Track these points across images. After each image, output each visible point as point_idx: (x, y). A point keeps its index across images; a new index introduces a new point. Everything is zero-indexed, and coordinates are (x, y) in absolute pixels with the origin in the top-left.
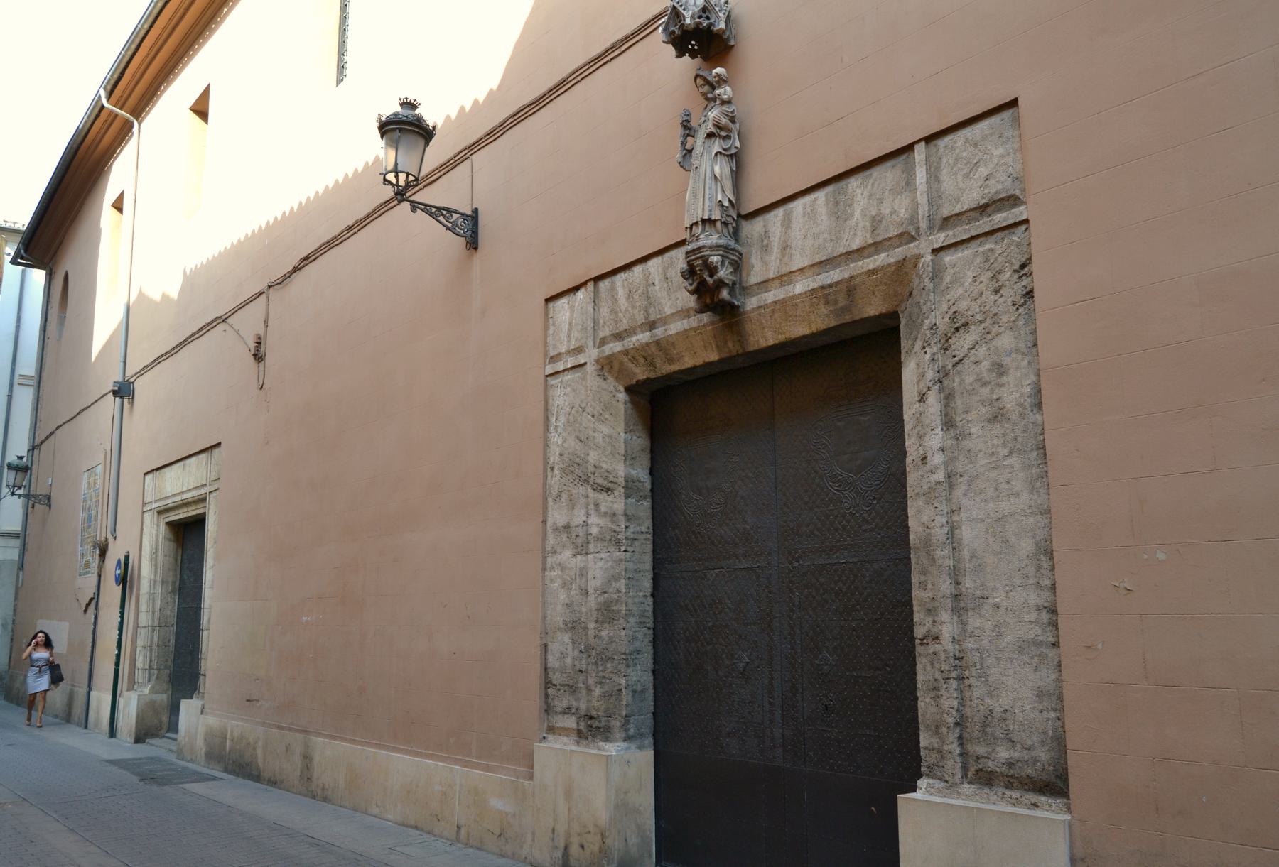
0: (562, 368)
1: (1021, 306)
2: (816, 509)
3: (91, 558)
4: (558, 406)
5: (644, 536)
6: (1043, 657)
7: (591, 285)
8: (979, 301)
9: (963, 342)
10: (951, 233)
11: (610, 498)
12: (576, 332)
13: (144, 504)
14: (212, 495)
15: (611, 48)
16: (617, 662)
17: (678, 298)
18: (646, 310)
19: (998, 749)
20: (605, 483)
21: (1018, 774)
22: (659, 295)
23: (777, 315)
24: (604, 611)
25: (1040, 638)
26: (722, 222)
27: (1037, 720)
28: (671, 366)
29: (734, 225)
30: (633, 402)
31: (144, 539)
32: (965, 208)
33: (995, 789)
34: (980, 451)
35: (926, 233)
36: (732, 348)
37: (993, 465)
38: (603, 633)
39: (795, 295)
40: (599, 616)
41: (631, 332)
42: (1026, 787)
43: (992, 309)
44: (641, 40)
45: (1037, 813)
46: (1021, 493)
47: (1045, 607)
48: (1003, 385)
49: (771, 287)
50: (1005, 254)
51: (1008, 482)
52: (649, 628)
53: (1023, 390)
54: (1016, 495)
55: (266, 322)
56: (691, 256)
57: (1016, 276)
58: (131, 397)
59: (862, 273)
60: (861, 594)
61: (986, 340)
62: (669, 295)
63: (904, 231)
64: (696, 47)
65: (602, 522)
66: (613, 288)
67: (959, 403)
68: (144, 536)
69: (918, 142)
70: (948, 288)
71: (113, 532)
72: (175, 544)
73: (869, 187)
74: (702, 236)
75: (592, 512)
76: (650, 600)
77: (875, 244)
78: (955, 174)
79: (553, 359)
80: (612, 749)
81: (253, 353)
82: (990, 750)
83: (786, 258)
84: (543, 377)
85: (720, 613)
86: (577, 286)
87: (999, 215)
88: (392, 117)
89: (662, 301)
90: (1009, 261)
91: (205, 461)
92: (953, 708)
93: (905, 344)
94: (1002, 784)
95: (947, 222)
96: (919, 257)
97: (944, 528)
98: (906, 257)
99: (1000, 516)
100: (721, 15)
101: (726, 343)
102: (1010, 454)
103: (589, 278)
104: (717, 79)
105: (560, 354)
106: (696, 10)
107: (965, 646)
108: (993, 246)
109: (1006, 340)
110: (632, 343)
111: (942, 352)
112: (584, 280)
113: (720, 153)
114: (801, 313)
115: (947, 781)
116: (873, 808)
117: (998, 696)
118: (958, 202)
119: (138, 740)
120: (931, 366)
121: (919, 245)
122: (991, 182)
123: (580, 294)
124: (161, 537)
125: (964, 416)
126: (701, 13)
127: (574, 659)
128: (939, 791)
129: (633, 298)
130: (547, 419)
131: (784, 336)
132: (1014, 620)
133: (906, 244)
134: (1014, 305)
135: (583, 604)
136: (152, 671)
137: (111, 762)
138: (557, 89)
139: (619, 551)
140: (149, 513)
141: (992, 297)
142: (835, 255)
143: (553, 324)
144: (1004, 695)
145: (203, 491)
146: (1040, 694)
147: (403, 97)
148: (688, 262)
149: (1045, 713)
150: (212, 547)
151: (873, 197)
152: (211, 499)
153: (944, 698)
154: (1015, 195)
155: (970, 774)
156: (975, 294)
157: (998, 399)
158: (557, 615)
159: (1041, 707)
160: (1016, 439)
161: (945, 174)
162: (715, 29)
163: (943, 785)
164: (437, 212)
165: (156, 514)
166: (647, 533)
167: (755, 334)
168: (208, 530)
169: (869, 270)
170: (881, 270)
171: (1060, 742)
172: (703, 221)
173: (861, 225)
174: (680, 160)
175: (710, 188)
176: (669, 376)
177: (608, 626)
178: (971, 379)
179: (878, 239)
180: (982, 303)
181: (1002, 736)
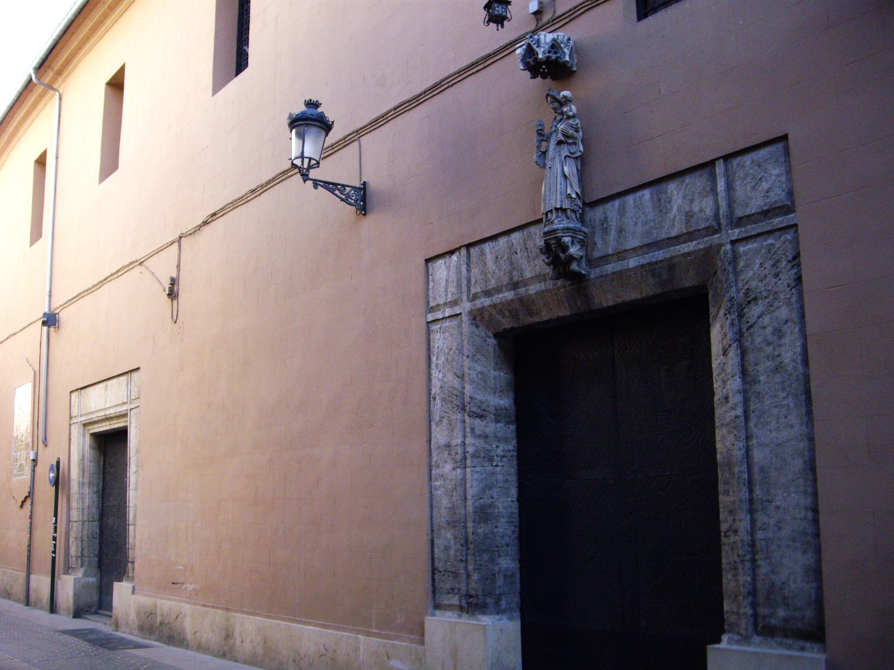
0: (441, 317)
1: (794, 287)
3: (24, 463)
5: (511, 453)
7: (464, 251)
9: (754, 311)
10: (743, 229)
12: (452, 288)
13: (71, 418)
14: (133, 412)
17: (536, 265)
18: (510, 272)
20: (479, 411)
26: (571, 210)
28: (532, 319)
29: (581, 211)
30: (499, 344)
31: (72, 448)
32: (753, 211)
34: (766, 394)
35: (725, 228)
37: (775, 405)
39: (629, 269)
41: (498, 290)
49: (610, 261)
50: (782, 248)
52: (516, 527)
53: (795, 350)
54: (792, 426)
55: (178, 267)
58: (57, 326)
61: (769, 311)
62: (528, 262)
64: (546, 70)
66: (482, 253)
67: (751, 357)
68: (72, 445)
71: (45, 442)
72: (98, 452)
74: (556, 221)
75: (468, 434)
76: (516, 504)
79: (432, 310)
80: (486, 620)
81: (167, 293)
83: (622, 239)
84: (424, 325)
87: (777, 219)
88: (299, 115)
90: (784, 254)
91: (125, 383)
92: (747, 582)
93: (712, 311)
95: (739, 222)
96: (720, 245)
100: (566, 50)
103: (462, 245)
104: (564, 99)
105: (439, 305)
106: (547, 47)
108: (773, 242)
110: (499, 299)
112: (458, 246)
113: (569, 156)
118: (747, 207)
119: (78, 613)
122: (771, 194)
123: (454, 257)
124: (86, 446)
125: (755, 367)
126: (551, 49)
127: (457, 551)
128: (737, 642)
129: (499, 263)
130: (429, 359)
131: (621, 299)
134: (789, 286)
136: (84, 558)
137: (65, 632)
139: (492, 466)
140: (77, 425)
141: (773, 279)
142: (658, 240)
143: (433, 281)
145: (124, 408)
147: (307, 99)
148: (545, 241)
150: (135, 456)
151: (686, 197)
152: (132, 415)
153: (741, 574)
154: (787, 205)
155: (759, 629)
158: (442, 515)
160: (791, 386)
161: (738, 185)
162: (561, 61)
164: (331, 186)
165: (82, 426)
166: (513, 450)
168: (130, 442)
169: (684, 253)
171: (819, 602)
172: (557, 209)
173: (677, 218)
174: (536, 160)
175: (561, 184)
176: (530, 326)
177: (483, 525)
179: (691, 230)
180: (766, 284)
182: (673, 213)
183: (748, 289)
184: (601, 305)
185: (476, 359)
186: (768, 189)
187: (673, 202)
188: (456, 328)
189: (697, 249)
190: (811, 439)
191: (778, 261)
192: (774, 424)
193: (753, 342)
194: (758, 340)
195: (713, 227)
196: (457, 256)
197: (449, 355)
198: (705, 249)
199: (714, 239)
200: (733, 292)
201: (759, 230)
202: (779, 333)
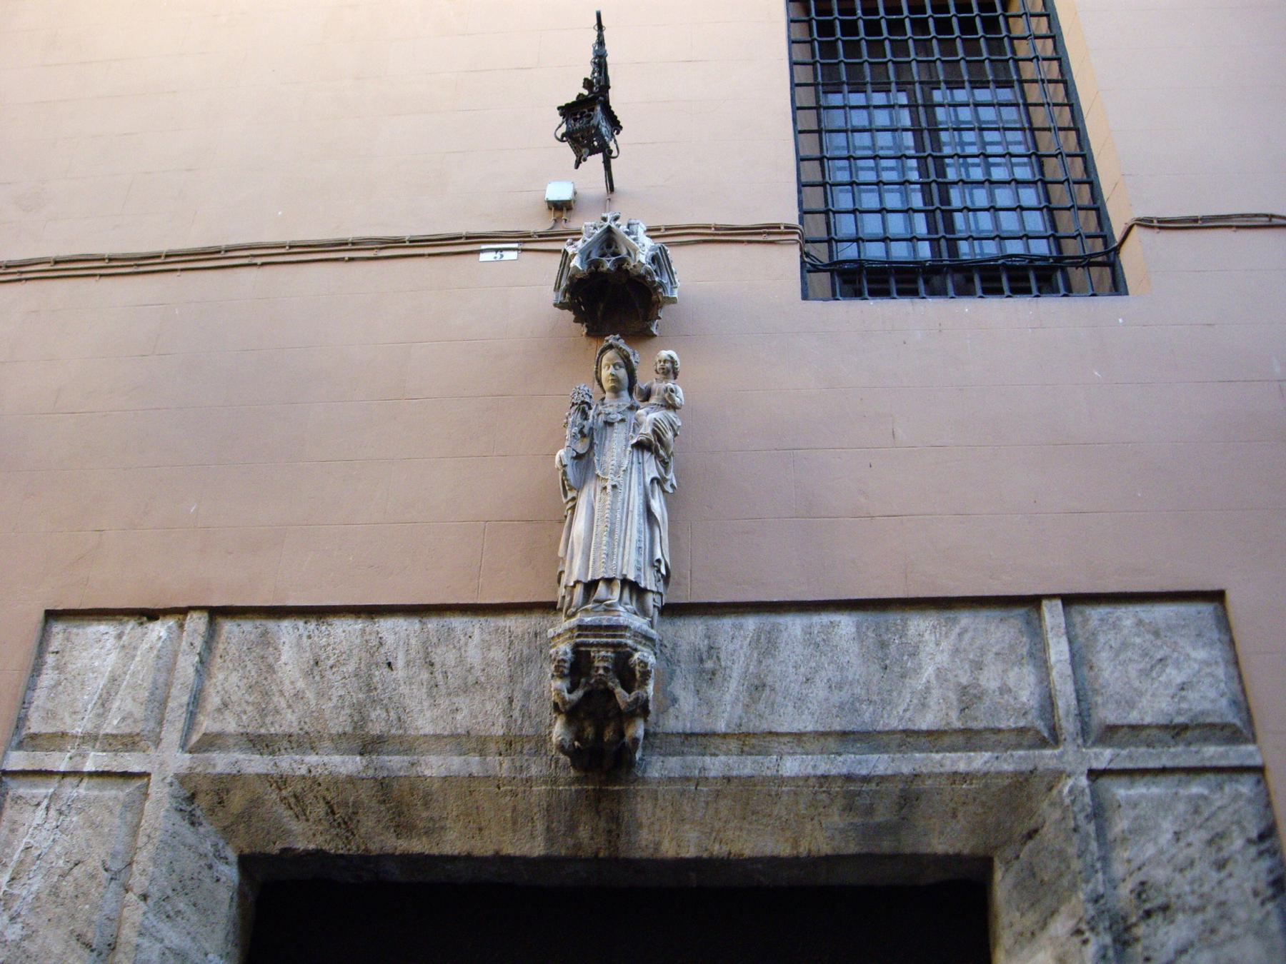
7: (197, 623)
8: (1189, 874)
12: (129, 702)
15: (353, 244)
18: (359, 708)
22: (404, 689)
23: (724, 804)
32: (1148, 720)
36: (588, 838)
44: (430, 255)
49: (717, 748)
50: (1230, 810)
56: (587, 636)
57: (1253, 851)
59: (941, 774)
63: (1029, 725)
69: (1051, 597)
73: (953, 636)
77: (967, 732)
78: (1123, 663)
79: (32, 742)
83: (761, 706)
86: (153, 610)
90: (1239, 823)
95: (1110, 734)
96: (1059, 775)
98: (1036, 769)
101: (572, 828)
105: (64, 735)
108: (1206, 792)
114: (784, 812)
122: (1191, 695)
123: (159, 629)
131: (725, 849)
133: (1030, 747)
138: (192, 258)
143: (59, 668)
154: (1234, 725)
169: (955, 773)
172: (625, 582)
173: (936, 693)
182: (924, 680)
183: (1143, 883)
184: (656, 850)
185: (168, 908)
186: (1184, 683)
188: (118, 809)
189: (993, 769)
191: (1220, 836)
195: (1038, 732)
196: (169, 628)
197: (69, 878)
198: (1017, 773)
199: (1042, 757)
201: (1166, 761)
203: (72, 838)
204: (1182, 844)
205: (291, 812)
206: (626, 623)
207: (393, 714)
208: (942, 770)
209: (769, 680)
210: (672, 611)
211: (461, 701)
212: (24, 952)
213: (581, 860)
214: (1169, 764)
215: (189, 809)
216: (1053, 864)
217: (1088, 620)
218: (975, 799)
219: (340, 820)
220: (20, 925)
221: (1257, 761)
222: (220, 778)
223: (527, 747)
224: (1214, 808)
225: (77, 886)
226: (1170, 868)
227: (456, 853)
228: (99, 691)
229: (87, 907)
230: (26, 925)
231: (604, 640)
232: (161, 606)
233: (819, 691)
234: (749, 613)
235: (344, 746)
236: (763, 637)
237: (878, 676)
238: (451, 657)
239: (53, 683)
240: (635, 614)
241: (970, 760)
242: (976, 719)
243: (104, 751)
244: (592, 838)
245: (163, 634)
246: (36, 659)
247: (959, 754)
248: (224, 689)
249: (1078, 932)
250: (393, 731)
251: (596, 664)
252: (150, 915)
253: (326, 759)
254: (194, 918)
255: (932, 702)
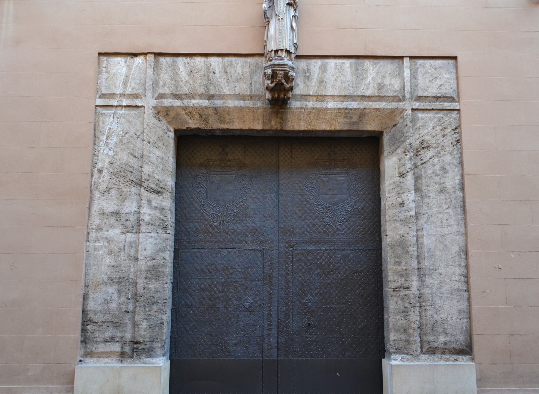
1: (455, 145)
2: (307, 221)
4: (110, 129)
6: (462, 296)
8: (435, 138)
9: (427, 154)
11: (160, 198)
16: (160, 305)
18: (206, 86)
19: (439, 337)
20: (156, 188)
21: (449, 347)
23: (312, 115)
24: (152, 272)
25: (461, 288)
27: (458, 323)
33: (436, 355)
34: (434, 204)
36: (274, 125)
37: (440, 211)
38: (151, 286)
40: (148, 275)
41: (191, 96)
42: (451, 353)
43: (441, 143)
45: (457, 363)
46: (453, 226)
47: (463, 275)
48: (445, 177)
50: (449, 121)
51: (447, 220)
54: (451, 226)
56: (276, 67)
57: (453, 132)
59: (372, 108)
60: (334, 266)
63: (397, 95)
65: (153, 213)
69: (406, 57)
70: (419, 128)
73: (377, 68)
78: (425, 78)
82: (436, 338)
83: (322, 87)
85: (231, 274)
87: (446, 104)
89: (222, 85)
90: (450, 125)
94: (440, 352)
95: (419, 98)
97: (414, 237)
99: (443, 234)
101: (270, 121)
102: (449, 207)
105: (114, 94)
107: (423, 292)
109: (448, 158)
111: (414, 156)
115: (412, 355)
116: (338, 374)
117: (440, 313)
120: (409, 162)
121: (405, 104)
122: (443, 88)
123: (139, 60)
131: (312, 127)
132: (449, 280)
133: (396, 102)
134: (452, 144)
135: (132, 266)
144: (443, 313)
146: (460, 312)
149: (462, 320)
154: (453, 97)
155: (424, 350)
156: (433, 134)
157: (443, 183)
159: (460, 317)
161: (419, 76)
163: (410, 357)
167: (293, 121)
170: (382, 110)
173: (372, 85)
177: (154, 282)
178: (430, 172)
181: (442, 331)
182: (368, 81)
185: (156, 145)
187: (369, 74)
189: (386, 108)
190: (466, 234)
192: (439, 223)
193: (425, 172)
194: (429, 172)
195: (399, 97)
196: (142, 59)
199: (399, 105)
200: (411, 140)
202: (444, 170)
203: (123, 126)
204: (434, 130)
205: (189, 117)
206: (287, 64)
207: (217, 89)
208: (372, 107)
209: (325, 80)
210: (298, 57)
211: (236, 84)
212: (115, 159)
213: (272, 130)
214: (434, 108)
215: (158, 116)
216: (400, 134)
217: (416, 64)
218: (380, 116)
219: (203, 119)
220: (113, 151)
221: (458, 108)
222: (166, 107)
223: (257, 98)
224: (444, 120)
225: (128, 139)
226: (430, 136)
227: (237, 128)
228: (122, 80)
229: (132, 146)
230: (114, 151)
231: (281, 69)
232: (138, 52)
233: (338, 84)
234: (319, 58)
235: (203, 97)
236: (323, 66)
237: (355, 79)
238: (232, 71)
239: (106, 77)
240: (289, 60)
241: (380, 105)
242: (382, 93)
243: (128, 99)
244: (275, 124)
245: (140, 61)
246: (98, 69)
247: (377, 103)
248: (163, 79)
249: (405, 152)
250: (217, 93)
251: (279, 76)
252: (151, 148)
253: (198, 101)
254: (164, 148)
255: (370, 87)
